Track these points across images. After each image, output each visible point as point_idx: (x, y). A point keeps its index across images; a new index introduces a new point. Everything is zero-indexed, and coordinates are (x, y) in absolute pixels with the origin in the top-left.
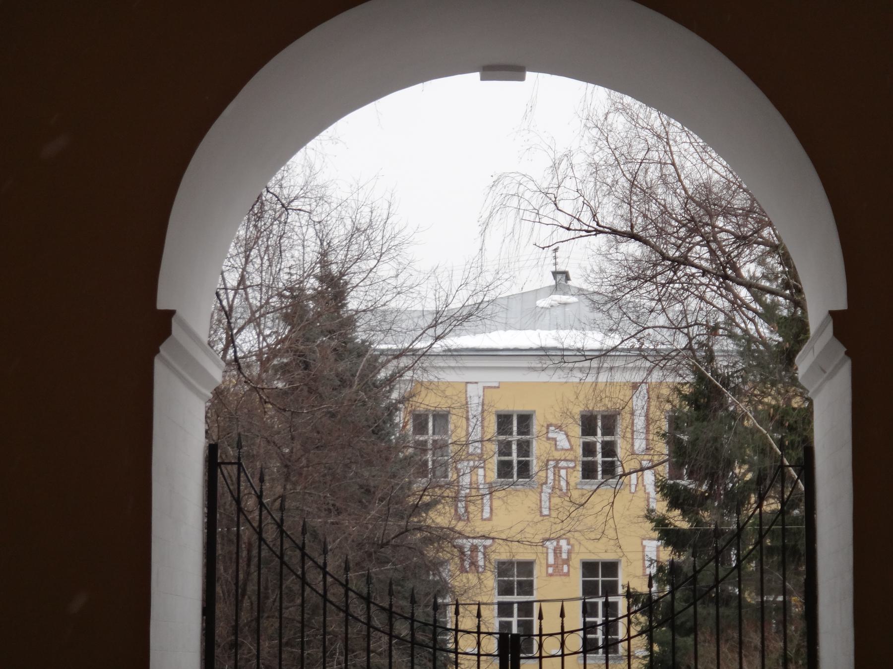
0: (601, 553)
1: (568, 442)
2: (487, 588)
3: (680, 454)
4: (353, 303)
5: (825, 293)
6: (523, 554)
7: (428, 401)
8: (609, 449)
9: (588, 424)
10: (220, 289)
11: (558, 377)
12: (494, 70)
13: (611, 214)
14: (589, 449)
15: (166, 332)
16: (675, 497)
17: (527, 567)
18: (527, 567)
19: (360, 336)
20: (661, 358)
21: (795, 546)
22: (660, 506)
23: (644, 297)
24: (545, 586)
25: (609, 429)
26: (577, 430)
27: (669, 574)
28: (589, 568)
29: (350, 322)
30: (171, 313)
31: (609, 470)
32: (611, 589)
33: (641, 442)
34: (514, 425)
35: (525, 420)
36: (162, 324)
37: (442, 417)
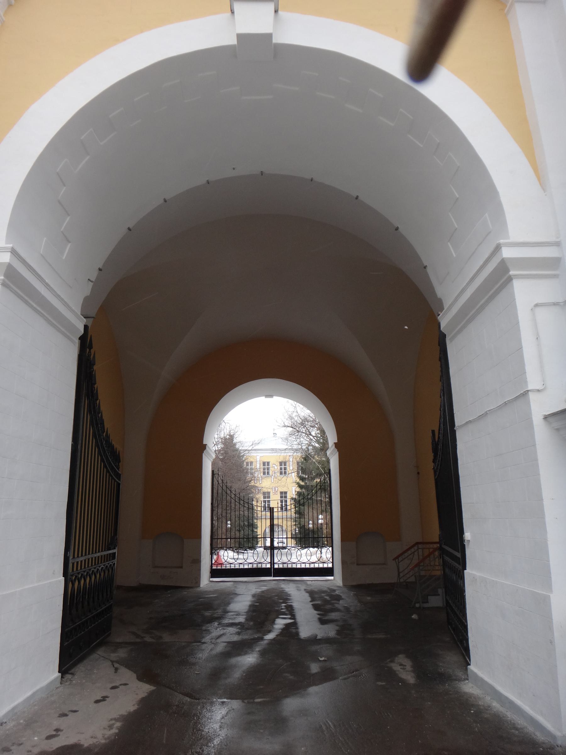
0: (284, 490)
1: (277, 468)
2: (261, 497)
3: (304, 471)
4: (235, 441)
5: (332, 438)
6: (269, 490)
7: (250, 460)
8: (285, 469)
9: (281, 464)
10: (213, 439)
11: (276, 454)
12: (268, 396)
13: (288, 423)
14: (281, 469)
15: (205, 448)
16: (302, 479)
17: (269, 493)
18: (269, 493)
19: (237, 446)
20: (296, 450)
21: (326, 488)
22: (298, 480)
23: (293, 438)
24: (273, 497)
25: (285, 465)
26: (279, 464)
27: (299, 494)
28: (281, 493)
29: (235, 444)
30: (206, 445)
31: (285, 473)
32: (286, 497)
33: (292, 467)
34: (266, 464)
35: (268, 463)
36: (204, 447)
37: (251, 463)
